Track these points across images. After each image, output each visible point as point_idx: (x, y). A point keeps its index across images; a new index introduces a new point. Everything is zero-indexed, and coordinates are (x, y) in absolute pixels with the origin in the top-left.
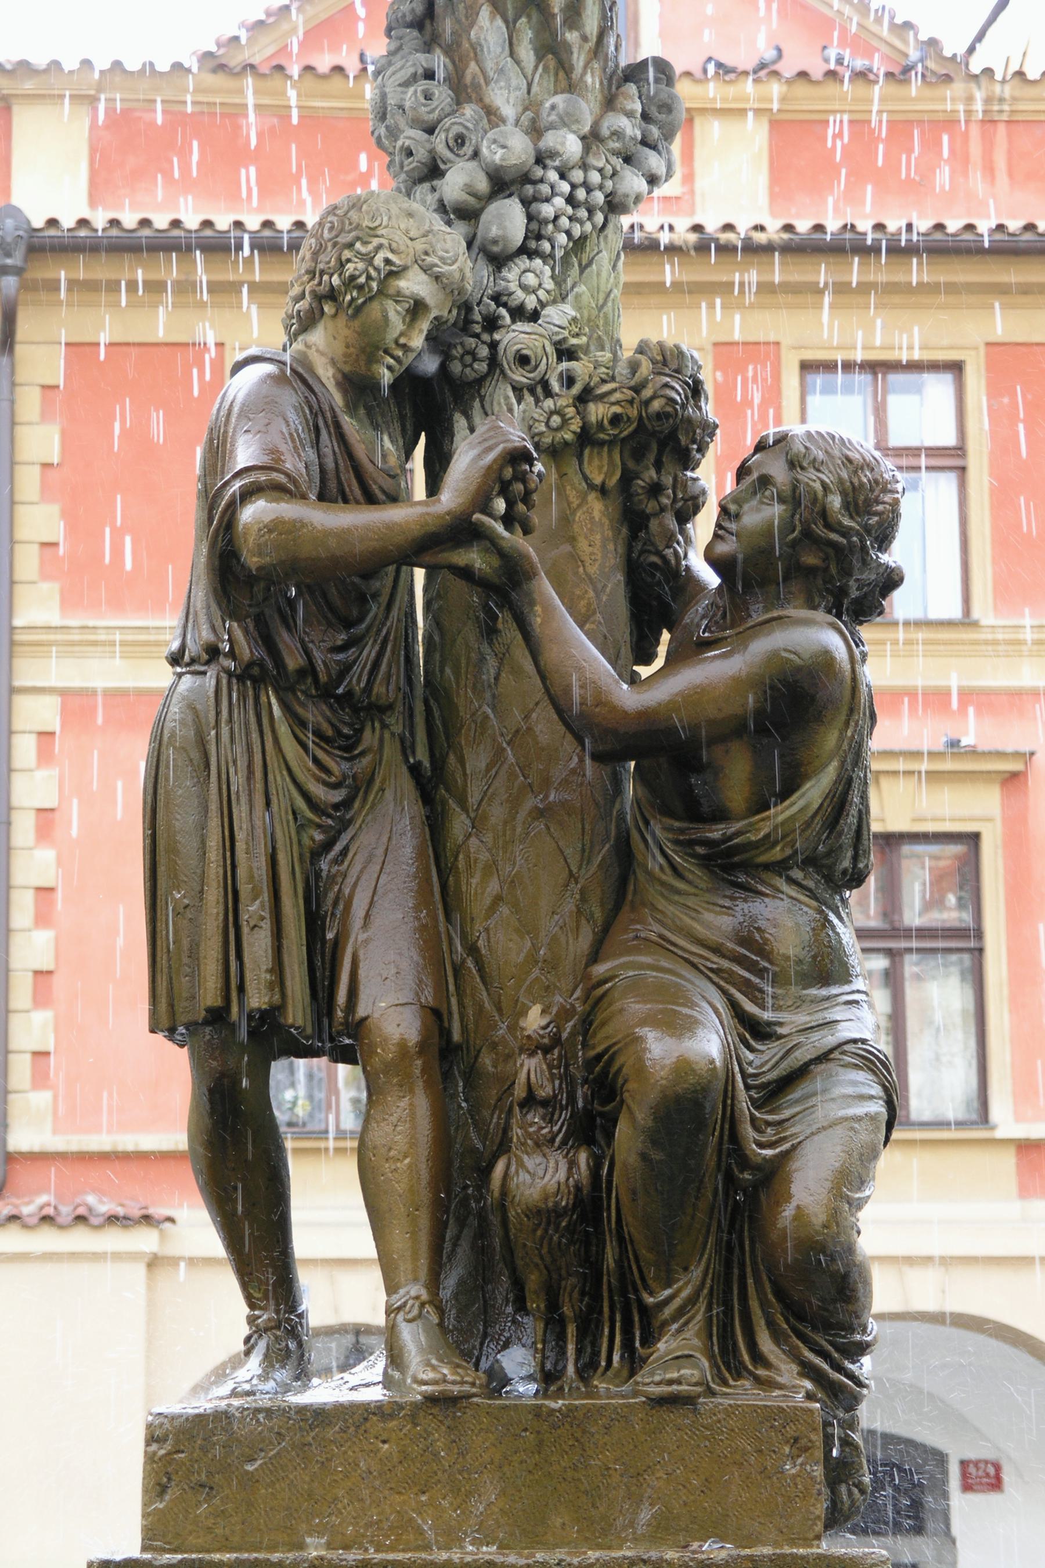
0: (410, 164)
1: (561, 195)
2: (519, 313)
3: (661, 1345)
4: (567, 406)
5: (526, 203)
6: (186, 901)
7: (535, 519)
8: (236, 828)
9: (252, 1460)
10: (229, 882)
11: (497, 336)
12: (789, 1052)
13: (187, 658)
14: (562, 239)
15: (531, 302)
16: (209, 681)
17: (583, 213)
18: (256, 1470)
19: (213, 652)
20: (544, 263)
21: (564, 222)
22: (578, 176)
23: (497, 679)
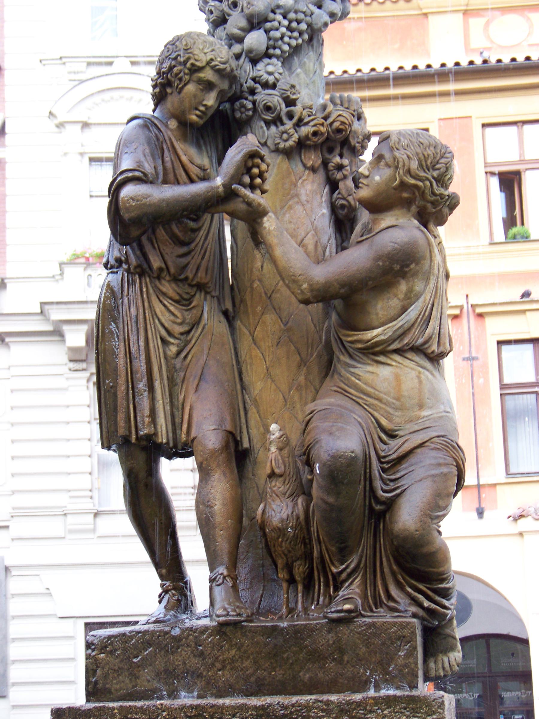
0: (212, 17)
1: (284, 26)
2: (266, 85)
3: (341, 593)
4: (290, 129)
5: (267, 32)
6: (111, 384)
7: (267, 186)
8: (131, 347)
9: (136, 657)
10: (129, 374)
11: (255, 97)
12: (403, 444)
13: (109, 266)
14: (286, 48)
15: (271, 79)
16: (119, 276)
17: (296, 34)
18: (139, 661)
19: (119, 262)
20: (278, 60)
21: (286, 39)
22: (292, 15)
23: (262, 267)
